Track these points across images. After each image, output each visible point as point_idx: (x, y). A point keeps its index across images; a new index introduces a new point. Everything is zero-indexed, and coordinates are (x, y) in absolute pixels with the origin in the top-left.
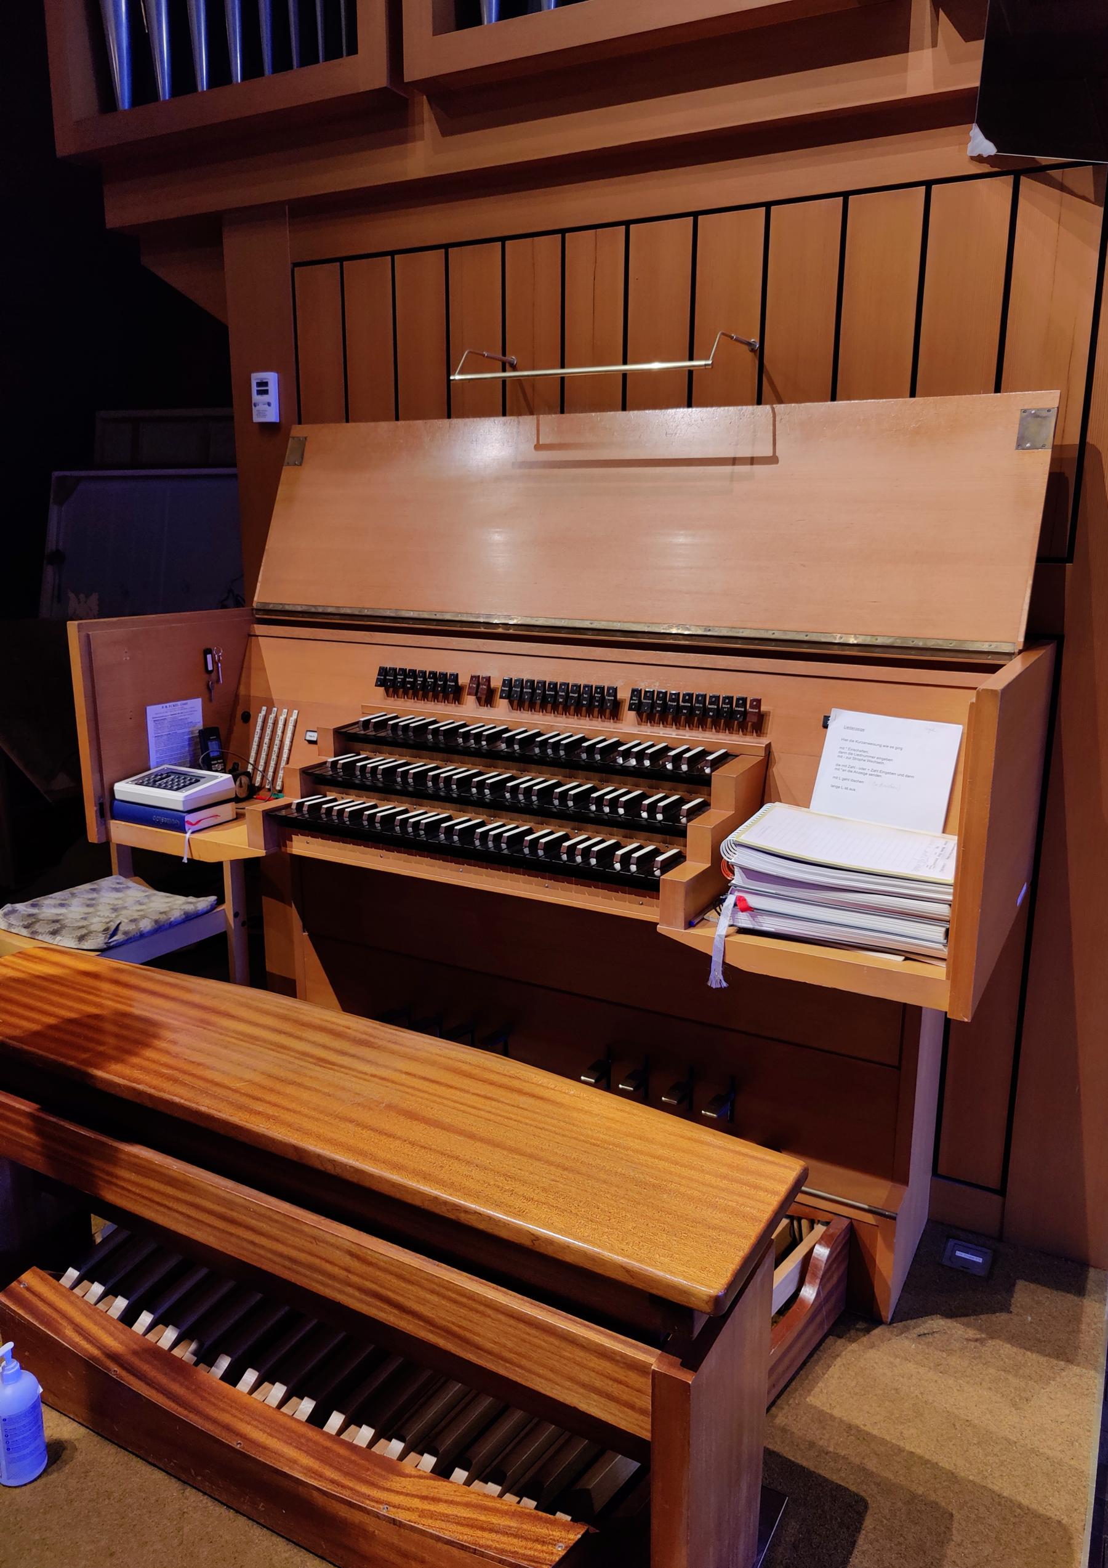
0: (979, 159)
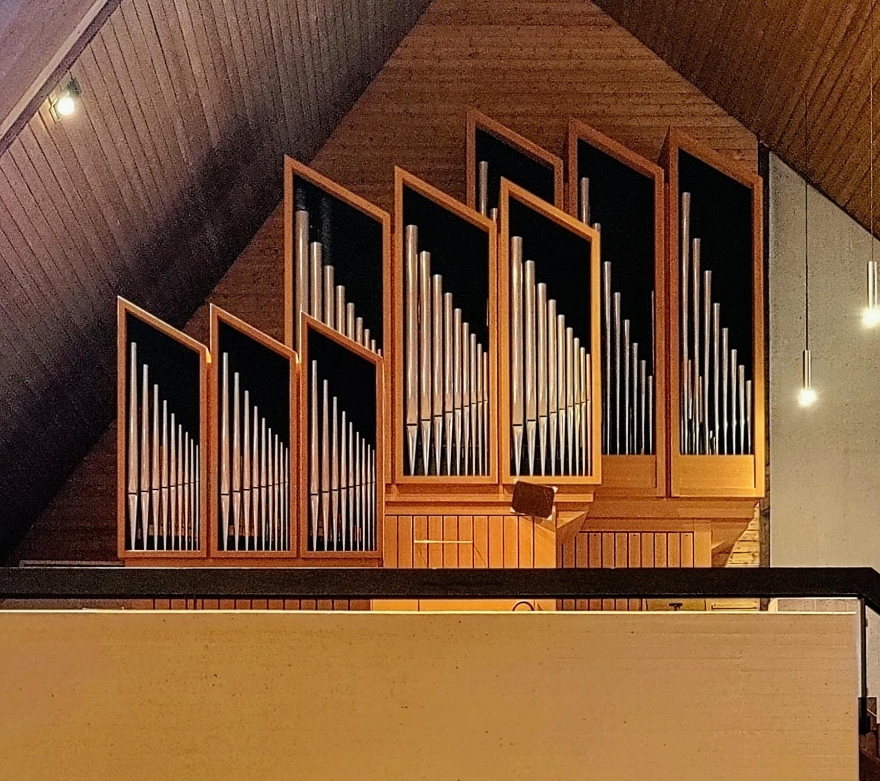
0: (512, 513)
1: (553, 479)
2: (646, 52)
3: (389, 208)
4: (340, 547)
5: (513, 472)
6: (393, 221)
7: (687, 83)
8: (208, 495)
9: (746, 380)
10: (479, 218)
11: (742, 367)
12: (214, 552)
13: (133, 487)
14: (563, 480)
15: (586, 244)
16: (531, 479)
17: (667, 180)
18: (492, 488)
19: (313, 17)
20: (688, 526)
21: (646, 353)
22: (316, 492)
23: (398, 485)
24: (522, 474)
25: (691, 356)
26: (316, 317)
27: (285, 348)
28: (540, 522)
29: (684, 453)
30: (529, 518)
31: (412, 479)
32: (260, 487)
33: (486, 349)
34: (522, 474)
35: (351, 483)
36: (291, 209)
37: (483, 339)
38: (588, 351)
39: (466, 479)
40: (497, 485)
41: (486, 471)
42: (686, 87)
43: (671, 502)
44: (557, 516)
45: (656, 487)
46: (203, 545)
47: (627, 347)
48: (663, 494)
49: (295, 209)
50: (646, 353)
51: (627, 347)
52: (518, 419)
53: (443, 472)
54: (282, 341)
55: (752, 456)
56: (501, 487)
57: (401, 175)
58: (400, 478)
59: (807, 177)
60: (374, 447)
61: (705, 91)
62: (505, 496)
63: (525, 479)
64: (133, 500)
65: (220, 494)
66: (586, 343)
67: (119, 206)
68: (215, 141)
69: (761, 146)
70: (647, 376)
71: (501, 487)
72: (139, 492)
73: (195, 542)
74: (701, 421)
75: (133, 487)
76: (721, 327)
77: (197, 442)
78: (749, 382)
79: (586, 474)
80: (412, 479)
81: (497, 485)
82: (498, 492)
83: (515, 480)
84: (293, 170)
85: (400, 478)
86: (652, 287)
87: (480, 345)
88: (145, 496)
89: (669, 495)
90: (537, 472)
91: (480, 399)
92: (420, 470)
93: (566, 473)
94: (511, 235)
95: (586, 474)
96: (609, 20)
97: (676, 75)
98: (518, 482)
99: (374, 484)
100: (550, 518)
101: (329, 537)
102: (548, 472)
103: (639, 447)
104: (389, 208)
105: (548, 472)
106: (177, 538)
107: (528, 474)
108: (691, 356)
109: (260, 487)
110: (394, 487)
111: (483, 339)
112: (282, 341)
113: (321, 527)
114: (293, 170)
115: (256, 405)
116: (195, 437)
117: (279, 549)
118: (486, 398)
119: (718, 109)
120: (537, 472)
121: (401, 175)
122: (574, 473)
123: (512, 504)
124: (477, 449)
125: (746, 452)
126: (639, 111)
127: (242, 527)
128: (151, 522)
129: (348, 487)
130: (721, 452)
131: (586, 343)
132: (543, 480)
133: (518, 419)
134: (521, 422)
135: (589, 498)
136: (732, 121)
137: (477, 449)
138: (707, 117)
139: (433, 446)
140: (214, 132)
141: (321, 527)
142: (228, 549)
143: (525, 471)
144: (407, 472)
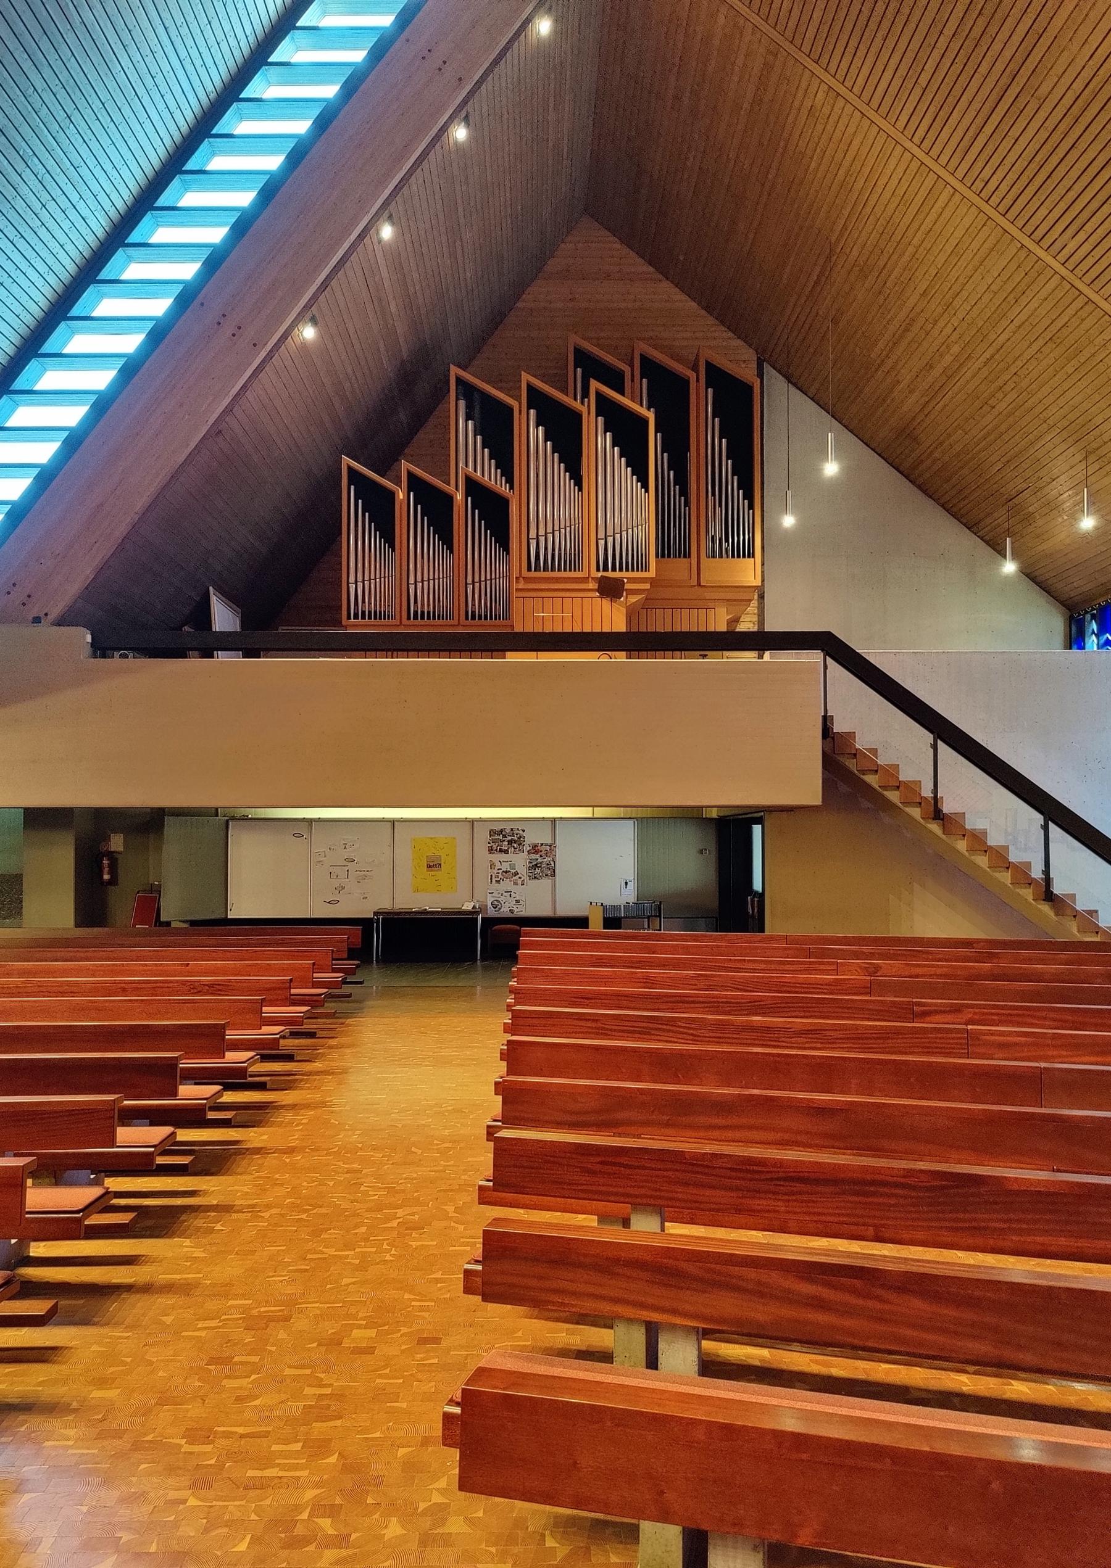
1: (624, 574)
2: (684, 297)
5: (598, 570)
7: (711, 318)
9: (749, 510)
10: (577, 405)
12: (405, 621)
13: (352, 579)
14: (630, 574)
15: (645, 422)
16: (610, 574)
17: (698, 380)
18: (585, 580)
20: (711, 605)
23: (524, 578)
24: (604, 570)
26: (470, 469)
27: (450, 489)
28: (615, 602)
30: (609, 599)
31: (533, 574)
32: (434, 579)
33: (580, 489)
34: (604, 570)
37: (579, 483)
38: (647, 491)
39: (568, 574)
40: (588, 578)
41: (581, 569)
42: (711, 320)
43: (701, 589)
44: (627, 598)
46: (398, 617)
47: (672, 489)
48: (695, 583)
49: (457, 399)
50: (684, 492)
52: (601, 535)
53: (553, 569)
54: (449, 485)
55: (752, 560)
56: (590, 579)
57: (526, 378)
58: (525, 573)
59: (789, 378)
60: (508, 553)
61: (723, 323)
62: (592, 585)
63: (606, 574)
66: (645, 486)
68: (405, 355)
69: (759, 358)
71: (590, 579)
72: (356, 582)
77: (393, 550)
79: (646, 571)
80: (533, 574)
81: (588, 578)
82: (588, 583)
83: (600, 574)
84: (456, 374)
85: (525, 573)
86: (688, 449)
88: (360, 585)
89: (699, 584)
90: (614, 569)
91: (577, 522)
92: (538, 568)
93: (633, 570)
95: (646, 571)
96: (660, 277)
97: (703, 312)
100: (622, 599)
102: (621, 569)
104: (518, 398)
105: (621, 569)
106: (380, 612)
107: (608, 570)
108: (713, 494)
109: (434, 579)
110: (521, 579)
111: (579, 483)
112: (449, 485)
113: (474, 605)
114: (456, 374)
117: (447, 619)
118: (580, 521)
119: (730, 334)
120: (614, 569)
121: (526, 378)
122: (638, 570)
123: (598, 590)
124: (575, 554)
125: (749, 557)
127: (423, 605)
131: (645, 486)
132: (617, 574)
133: (601, 535)
134: (604, 537)
135: (647, 586)
136: (739, 342)
137: (575, 554)
143: (606, 569)
144: (529, 569)
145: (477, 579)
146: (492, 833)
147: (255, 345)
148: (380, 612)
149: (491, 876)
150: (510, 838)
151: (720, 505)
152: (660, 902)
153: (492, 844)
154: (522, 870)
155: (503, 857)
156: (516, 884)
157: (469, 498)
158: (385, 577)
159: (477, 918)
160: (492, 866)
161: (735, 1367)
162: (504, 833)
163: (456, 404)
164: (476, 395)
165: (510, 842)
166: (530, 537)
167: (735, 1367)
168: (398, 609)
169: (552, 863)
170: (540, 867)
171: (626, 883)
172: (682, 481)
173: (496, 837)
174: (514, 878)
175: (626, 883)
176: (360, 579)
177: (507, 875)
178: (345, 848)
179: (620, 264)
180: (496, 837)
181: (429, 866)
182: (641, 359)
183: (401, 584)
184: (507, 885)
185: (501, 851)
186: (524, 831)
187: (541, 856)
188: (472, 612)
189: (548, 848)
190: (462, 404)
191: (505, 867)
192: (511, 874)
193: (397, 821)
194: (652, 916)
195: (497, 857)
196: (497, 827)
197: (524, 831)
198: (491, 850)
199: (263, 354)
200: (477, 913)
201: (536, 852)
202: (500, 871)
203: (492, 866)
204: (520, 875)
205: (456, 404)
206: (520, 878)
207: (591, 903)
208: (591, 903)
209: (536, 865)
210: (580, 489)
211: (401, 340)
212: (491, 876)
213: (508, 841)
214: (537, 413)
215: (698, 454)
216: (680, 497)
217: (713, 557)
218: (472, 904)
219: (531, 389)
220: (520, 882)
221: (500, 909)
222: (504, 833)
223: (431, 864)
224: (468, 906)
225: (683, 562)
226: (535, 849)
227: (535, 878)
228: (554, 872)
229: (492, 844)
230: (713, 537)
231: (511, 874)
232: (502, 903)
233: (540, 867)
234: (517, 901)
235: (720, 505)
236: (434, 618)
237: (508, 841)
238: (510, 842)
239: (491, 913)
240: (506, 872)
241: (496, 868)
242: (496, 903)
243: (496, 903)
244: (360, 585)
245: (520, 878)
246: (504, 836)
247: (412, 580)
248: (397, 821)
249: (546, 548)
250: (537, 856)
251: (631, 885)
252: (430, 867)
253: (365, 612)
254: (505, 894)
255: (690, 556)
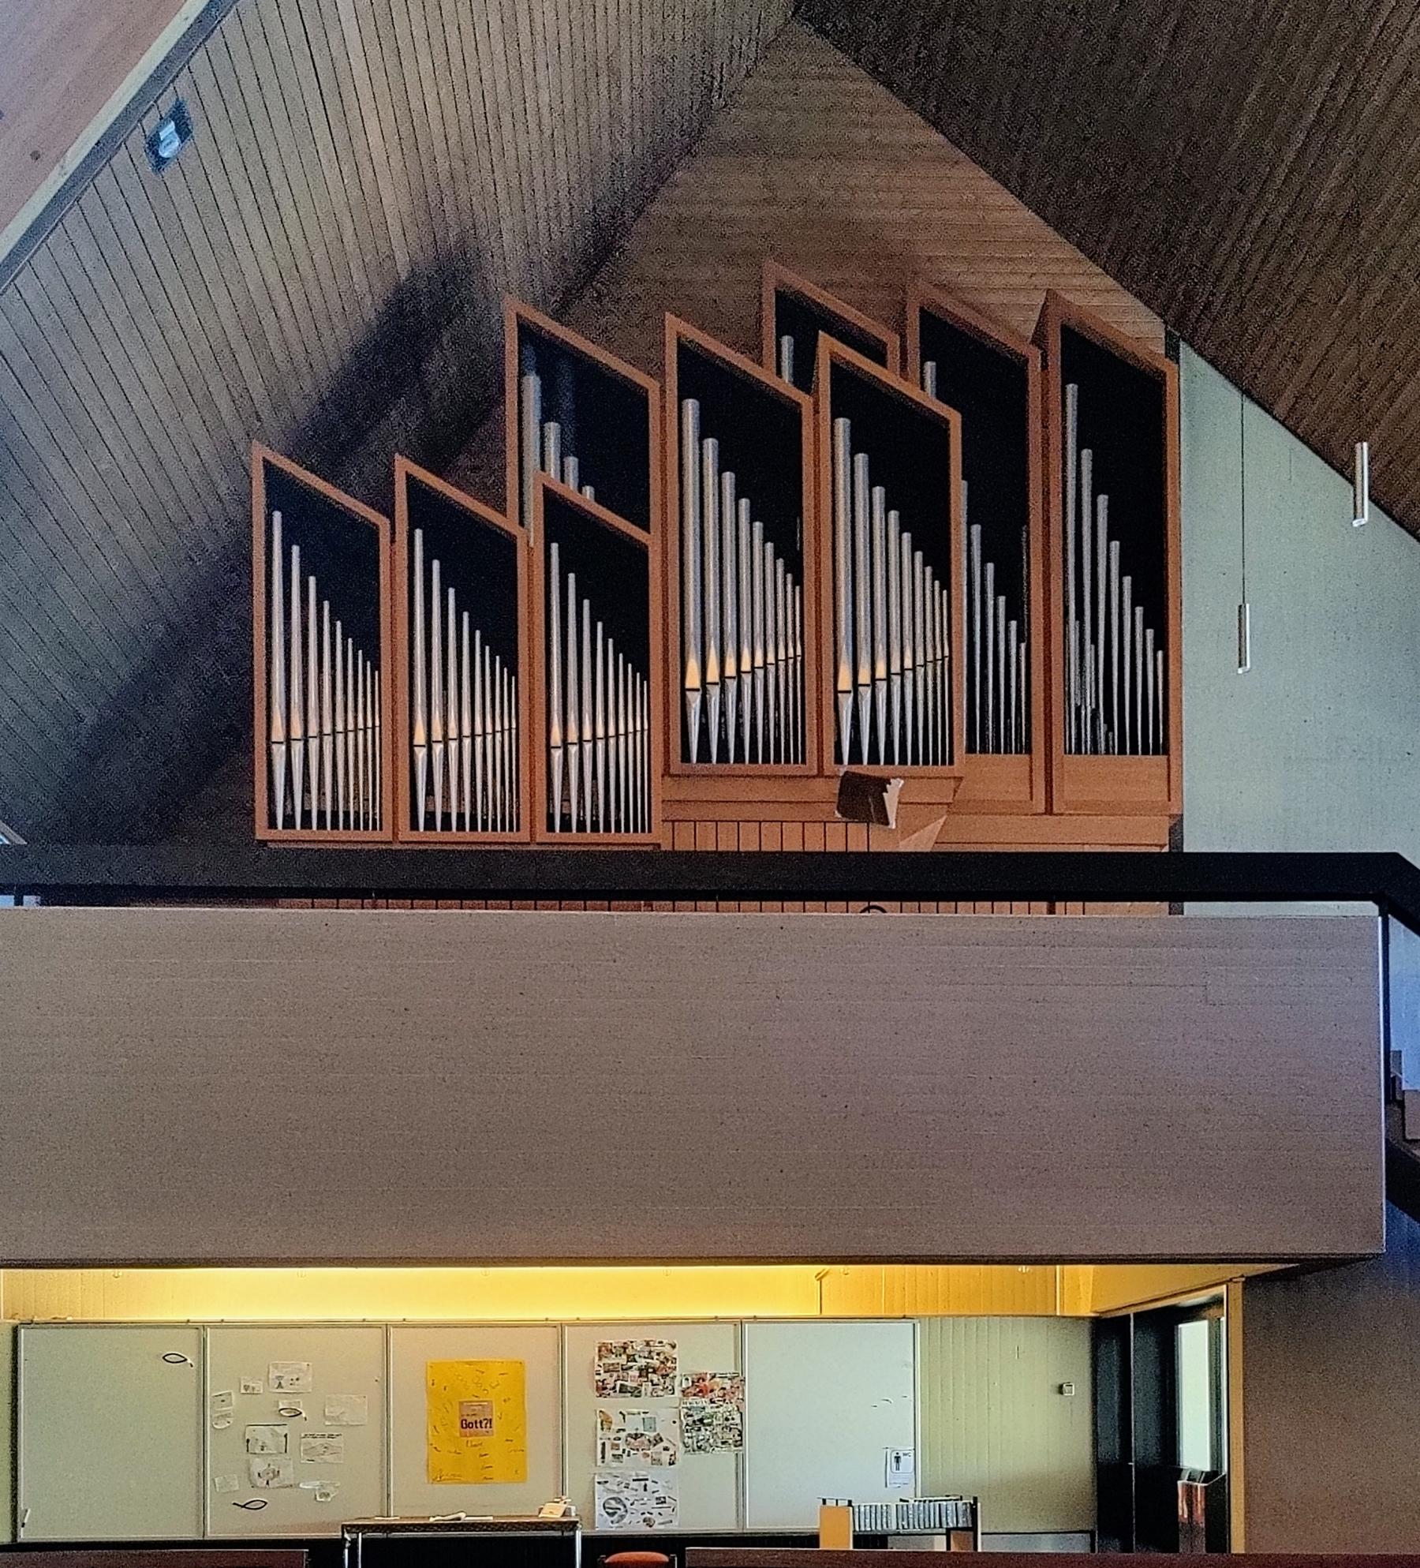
2: (1012, 200)
3: (660, 374)
4: (595, 827)
6: (663, 391)
7: (1069, 247)
8: (394, 743)
10: (784, 384)
11: (1150, 633)
13: (278, 734)
15: (940, 427)
16: (865, 768)
19: (544, 98)
21: (1017, 610)
22: (559, 744)
25: (1080, 615)
27: (507, 523)
29: (1070, 752)
32: (473, 736)
33: (798, 581)
35: (612, 732)
36: (516, 372)
37: (795, 567)
42: (1068, 251)
45: (1031, 799)
47: (990, 603)
50: (1017, 610)
51: (990, 603)
54: (503, 512)
55: (1165, 757)
57: (674, 326)
59: (1233, 375)
64: (279, 752)
65: (412, 746)
67: (255, 339)
69: (1168, 334)
70: (1019, 642)
72: (288, 740)
73: (374, 820)
74: (1094, 706)
75: (278, 734)
76: (1121, 575)
77: (376, 667)
78: (1160, 654)
84: (518, 316)
86: (1025, 521)
87: (789, 577)
88: (297, 748)
94: (834, 416)
97: (1050, 233)
98: (846, 773)
99: (646, 733)
101: (578, 815)
103: (1008, 743)
104: (660, 374)
106: (347, 814)
108: (1080, 615)
109: (473, 736)
112: (503, 512)
113: (566, 799)
115: (468, 610)
116: (373, 656)
119: (1110, 281)
121: (674, 326)
125: (1156, 752)
126: (998, 281)
128: (306, 789)
129: (606, 737)
130: (1122, 751)
132: (880, 770)
138: (1096, 291)
139: (723, 721)
140: (402, 259)
141: (566, 799)
142: (426, 829)
145: (573, 736)
146: (604, 1350)
147: (36, 156)
148: (347, 814)
149: (604, 1444)
150: (642, 1362)
151: (1094, 640)
152: (975, 1499)
153: (604, 1376)
154: (671, 1433)
155: (627, 1403)
156: (657, 1462)
157: (555, 546)
158: (356, 730)
159: (573, 1539)
160: (606, 1422)
161: (66, 902)
162: (629, 1351)
163: (520, 384)
164: (564, 366)
165: (644, 1372)
166: (688, 686)
167: (66, 902)
168: (388, 806)
169: (737, 1416)
170: (709, 1425)
171: (898, 1459)
172: (1012, 584)
173: (613, 1360)
174: (653, 1449)
175: (898, 1459)
176: (297, 731)
177: (636, 1443)
178: (280, 1386)
179: (871, 126)
180: (613, 1360)
181: (466, 1425)
182: (921, 318)
183: (395, 768)
184: (635, 1464)
185: (623, 1389)
186: (674, 1347)
187: (712, 1402)
188: (563, 816)
189: (727, 1384)
190: (533, 382)
191: (633, 1425)
192: (642, 1441)
193: (395, 1327)
194: (956, 1529)
195: (614, 1404)
196: (615, 1339)
197: (674, 1347)
198: (602, 1389)
199: (55, 182)
200: (573, 1526)
201: (702, 1392)
202: (623, 1435)
203: (606, 1422)
204: (664, 1444)
205: (520, 384)
206: (666, 1449)
207: (824, 1501)
208: (824, 1501)
209: (701, 1420)
210: (798, 581)
211: (395, 230)
212: (604, 1444)
213: (640, 1370)
214: (701, 409)
215: (1047, 535)
216: (1007, 621)
217: (1079, 751)
218: (562, 1507)
219: (689, 355)
220: (665, 1457)
221: (622, 1517)
222: (629, 1351)
223: (469, 1420)
224: (553, 1512)
225: (1015, 762)
226: (699, 1386)
227: (699, 1448)
228: (740, 1435)
229: (604, 1376)
230: (1078, 709)
231: (642, 1441)
232: (628, 1504)
233: (709, 1425)
234: (661, 1501)
235: (1094, 640)
236: (473, 828)
237: (640, 1370)
238: (644, 1372)
239: (604, 1526)
240: (636, 1437)
241: (614, 1427)
242: (613, 1504)
243: (613, 1504)
244: (297, 748)
245: (666, 1449)
246: (631, 1358)
247: (420, 737)
248: (395, 1327)
249: (723, 713)
250: (703, 1402)
251: (907, 1462)
252: (468, 1426)
253: (310, 812)
254: (634, 1485)
255: (1029, 751)
